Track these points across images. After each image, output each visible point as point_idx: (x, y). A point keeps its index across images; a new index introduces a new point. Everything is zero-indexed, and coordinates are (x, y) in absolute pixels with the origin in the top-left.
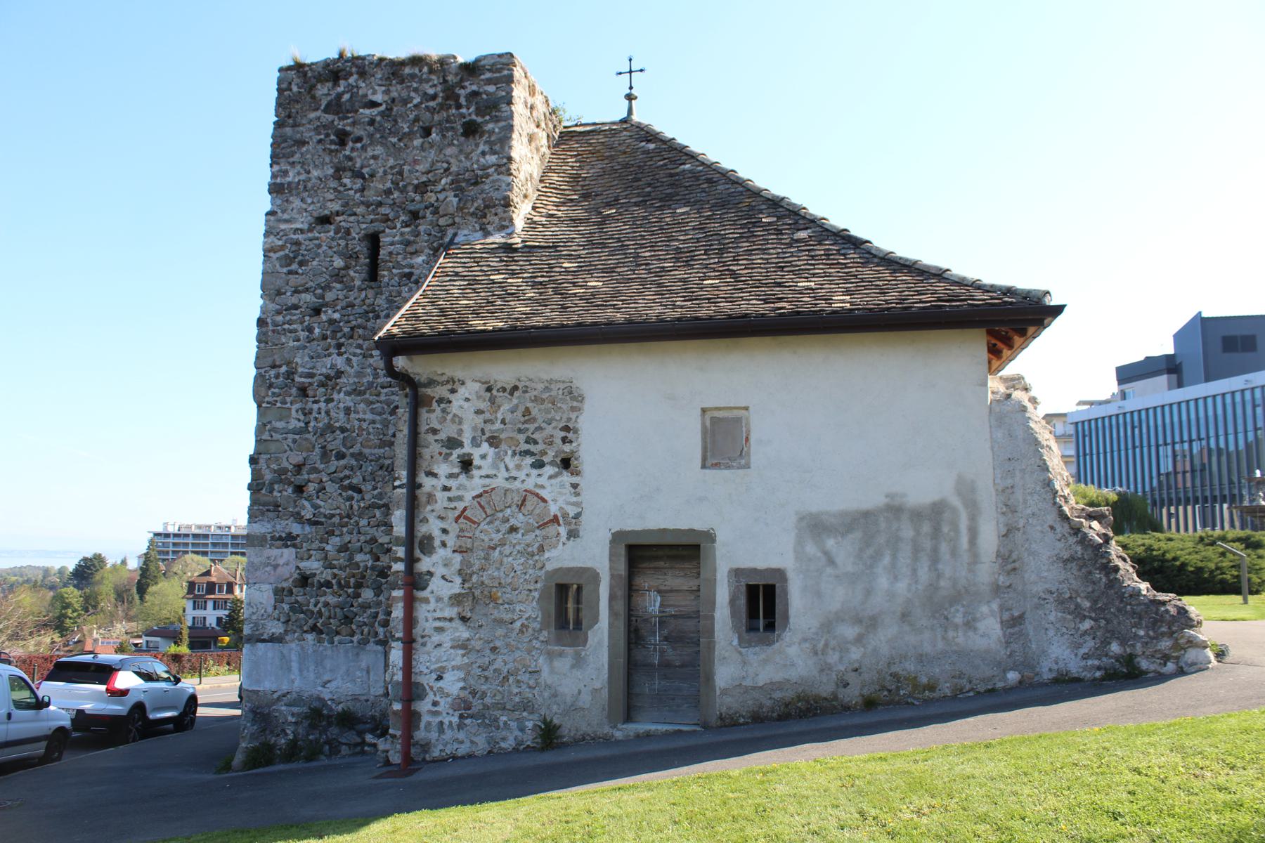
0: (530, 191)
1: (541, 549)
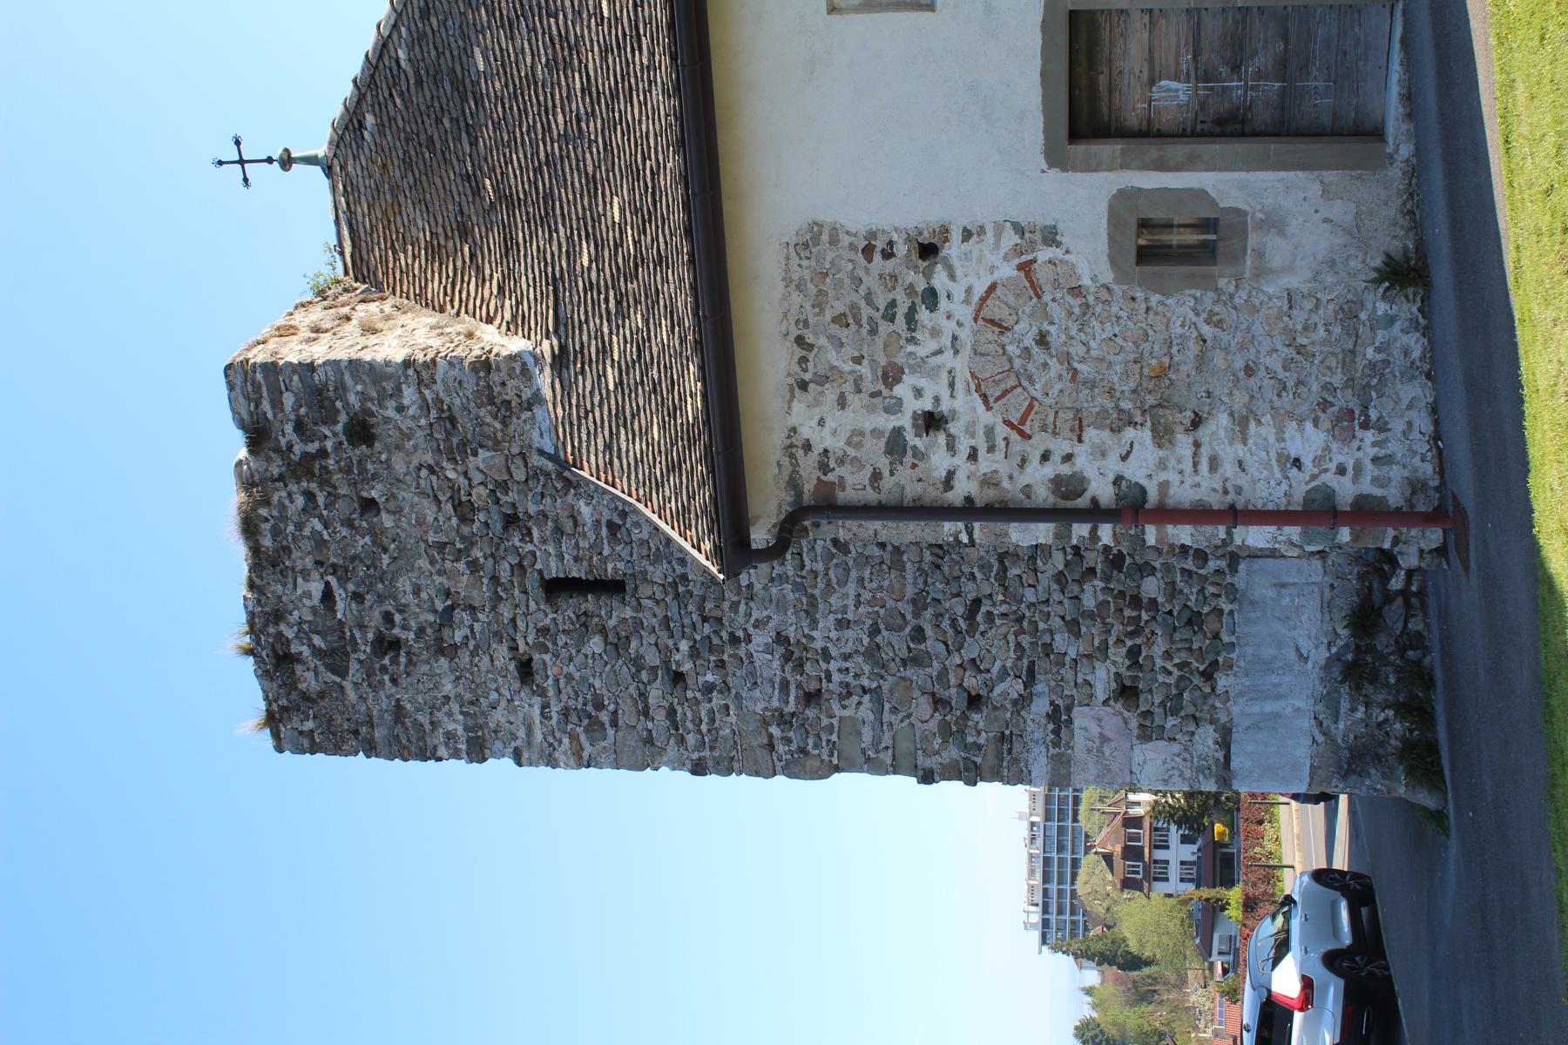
0: (459, 328)
1: (1076, 291)
